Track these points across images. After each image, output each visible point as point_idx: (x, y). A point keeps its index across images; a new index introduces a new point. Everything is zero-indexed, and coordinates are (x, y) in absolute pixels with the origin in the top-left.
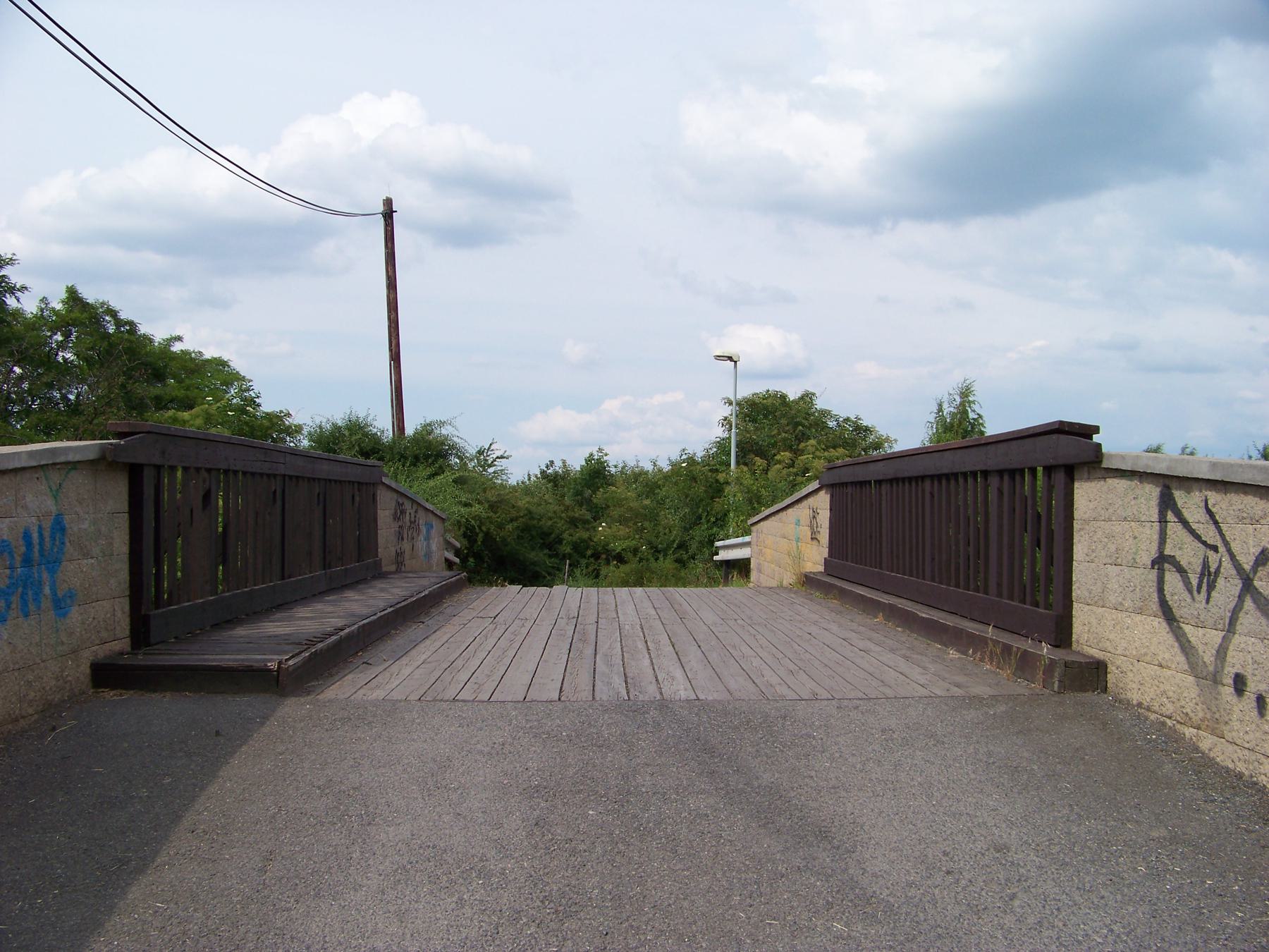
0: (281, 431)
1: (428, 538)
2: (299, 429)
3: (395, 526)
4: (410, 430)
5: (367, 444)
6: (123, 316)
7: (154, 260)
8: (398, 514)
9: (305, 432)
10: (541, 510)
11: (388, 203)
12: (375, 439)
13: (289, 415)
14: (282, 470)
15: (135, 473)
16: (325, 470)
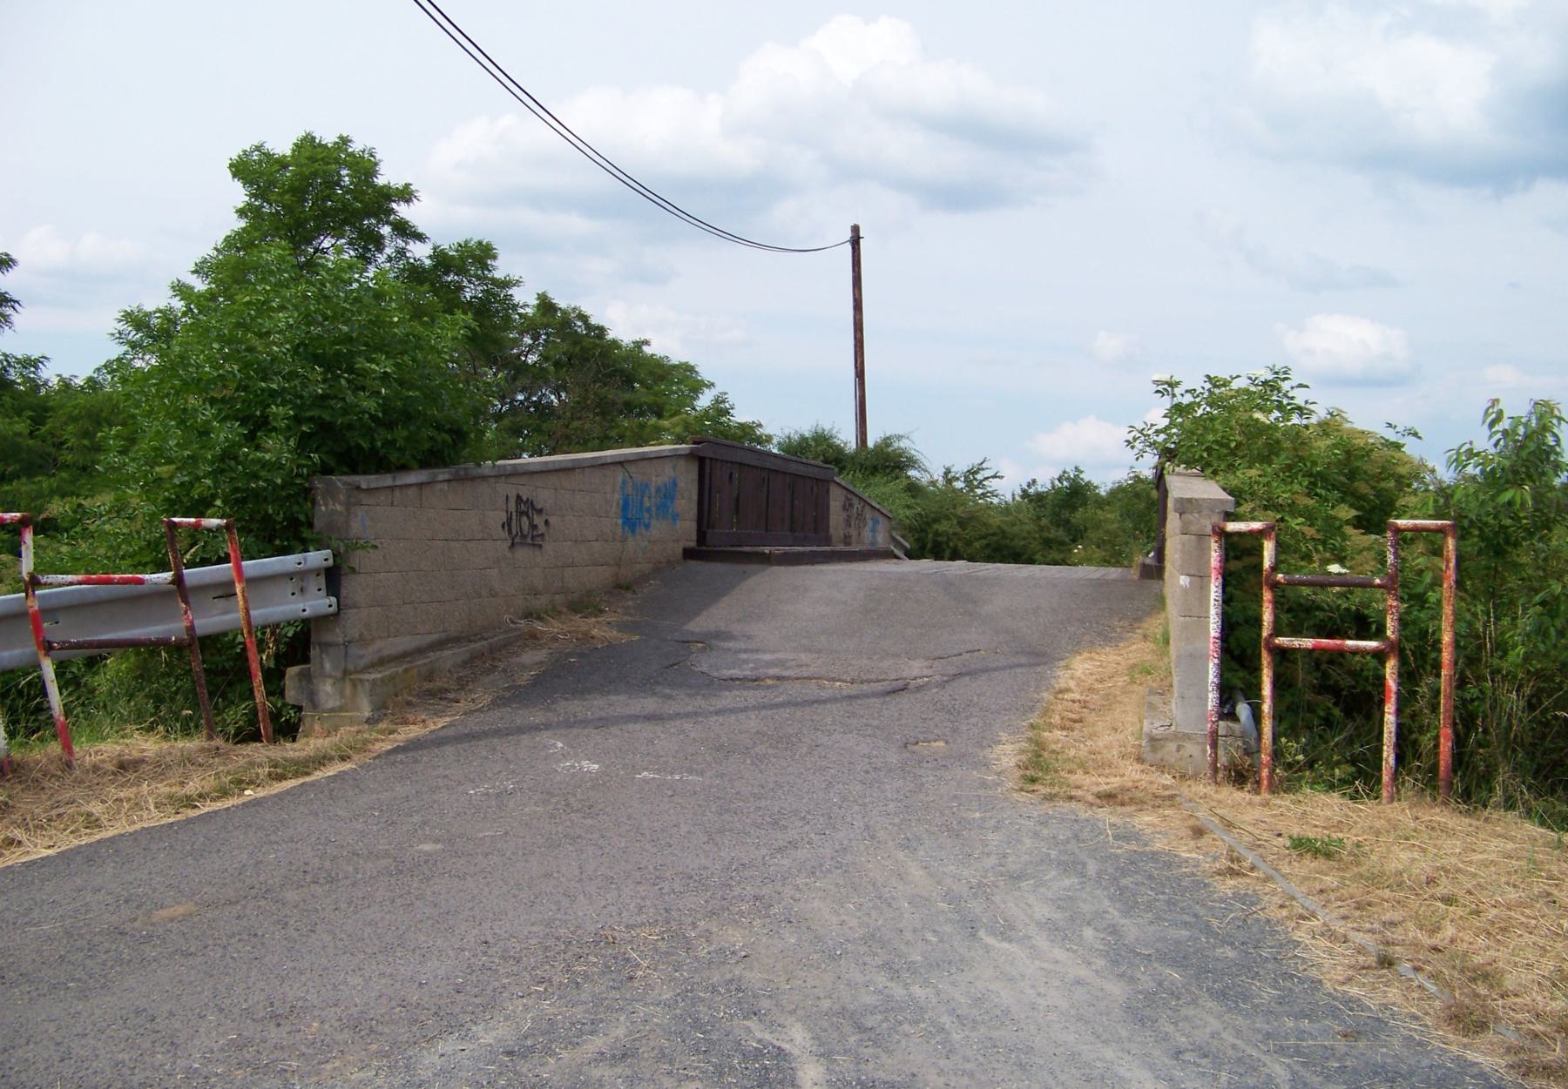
0: (752, 440)
1: (874, 530)
2: (769, 439)
3: (844, 515)
4: (870, 444)
5: (831, 454)
6: (593, 321)
7: (578, 224)
8: (847, 506)
9: (775, 441)
10: (1016, 529)
11: (856, 229)
12: (839, 450)
13: (760, 425)
14: (768, 465)
15: (702, 461)
16: (793, 468)
